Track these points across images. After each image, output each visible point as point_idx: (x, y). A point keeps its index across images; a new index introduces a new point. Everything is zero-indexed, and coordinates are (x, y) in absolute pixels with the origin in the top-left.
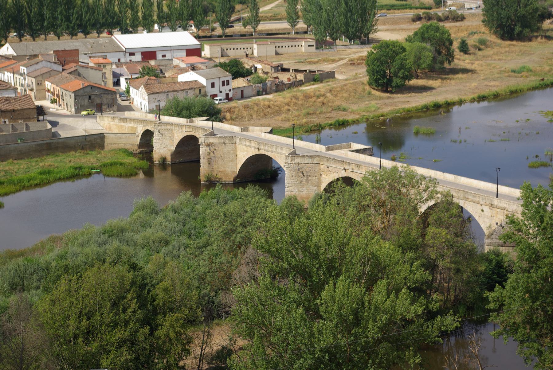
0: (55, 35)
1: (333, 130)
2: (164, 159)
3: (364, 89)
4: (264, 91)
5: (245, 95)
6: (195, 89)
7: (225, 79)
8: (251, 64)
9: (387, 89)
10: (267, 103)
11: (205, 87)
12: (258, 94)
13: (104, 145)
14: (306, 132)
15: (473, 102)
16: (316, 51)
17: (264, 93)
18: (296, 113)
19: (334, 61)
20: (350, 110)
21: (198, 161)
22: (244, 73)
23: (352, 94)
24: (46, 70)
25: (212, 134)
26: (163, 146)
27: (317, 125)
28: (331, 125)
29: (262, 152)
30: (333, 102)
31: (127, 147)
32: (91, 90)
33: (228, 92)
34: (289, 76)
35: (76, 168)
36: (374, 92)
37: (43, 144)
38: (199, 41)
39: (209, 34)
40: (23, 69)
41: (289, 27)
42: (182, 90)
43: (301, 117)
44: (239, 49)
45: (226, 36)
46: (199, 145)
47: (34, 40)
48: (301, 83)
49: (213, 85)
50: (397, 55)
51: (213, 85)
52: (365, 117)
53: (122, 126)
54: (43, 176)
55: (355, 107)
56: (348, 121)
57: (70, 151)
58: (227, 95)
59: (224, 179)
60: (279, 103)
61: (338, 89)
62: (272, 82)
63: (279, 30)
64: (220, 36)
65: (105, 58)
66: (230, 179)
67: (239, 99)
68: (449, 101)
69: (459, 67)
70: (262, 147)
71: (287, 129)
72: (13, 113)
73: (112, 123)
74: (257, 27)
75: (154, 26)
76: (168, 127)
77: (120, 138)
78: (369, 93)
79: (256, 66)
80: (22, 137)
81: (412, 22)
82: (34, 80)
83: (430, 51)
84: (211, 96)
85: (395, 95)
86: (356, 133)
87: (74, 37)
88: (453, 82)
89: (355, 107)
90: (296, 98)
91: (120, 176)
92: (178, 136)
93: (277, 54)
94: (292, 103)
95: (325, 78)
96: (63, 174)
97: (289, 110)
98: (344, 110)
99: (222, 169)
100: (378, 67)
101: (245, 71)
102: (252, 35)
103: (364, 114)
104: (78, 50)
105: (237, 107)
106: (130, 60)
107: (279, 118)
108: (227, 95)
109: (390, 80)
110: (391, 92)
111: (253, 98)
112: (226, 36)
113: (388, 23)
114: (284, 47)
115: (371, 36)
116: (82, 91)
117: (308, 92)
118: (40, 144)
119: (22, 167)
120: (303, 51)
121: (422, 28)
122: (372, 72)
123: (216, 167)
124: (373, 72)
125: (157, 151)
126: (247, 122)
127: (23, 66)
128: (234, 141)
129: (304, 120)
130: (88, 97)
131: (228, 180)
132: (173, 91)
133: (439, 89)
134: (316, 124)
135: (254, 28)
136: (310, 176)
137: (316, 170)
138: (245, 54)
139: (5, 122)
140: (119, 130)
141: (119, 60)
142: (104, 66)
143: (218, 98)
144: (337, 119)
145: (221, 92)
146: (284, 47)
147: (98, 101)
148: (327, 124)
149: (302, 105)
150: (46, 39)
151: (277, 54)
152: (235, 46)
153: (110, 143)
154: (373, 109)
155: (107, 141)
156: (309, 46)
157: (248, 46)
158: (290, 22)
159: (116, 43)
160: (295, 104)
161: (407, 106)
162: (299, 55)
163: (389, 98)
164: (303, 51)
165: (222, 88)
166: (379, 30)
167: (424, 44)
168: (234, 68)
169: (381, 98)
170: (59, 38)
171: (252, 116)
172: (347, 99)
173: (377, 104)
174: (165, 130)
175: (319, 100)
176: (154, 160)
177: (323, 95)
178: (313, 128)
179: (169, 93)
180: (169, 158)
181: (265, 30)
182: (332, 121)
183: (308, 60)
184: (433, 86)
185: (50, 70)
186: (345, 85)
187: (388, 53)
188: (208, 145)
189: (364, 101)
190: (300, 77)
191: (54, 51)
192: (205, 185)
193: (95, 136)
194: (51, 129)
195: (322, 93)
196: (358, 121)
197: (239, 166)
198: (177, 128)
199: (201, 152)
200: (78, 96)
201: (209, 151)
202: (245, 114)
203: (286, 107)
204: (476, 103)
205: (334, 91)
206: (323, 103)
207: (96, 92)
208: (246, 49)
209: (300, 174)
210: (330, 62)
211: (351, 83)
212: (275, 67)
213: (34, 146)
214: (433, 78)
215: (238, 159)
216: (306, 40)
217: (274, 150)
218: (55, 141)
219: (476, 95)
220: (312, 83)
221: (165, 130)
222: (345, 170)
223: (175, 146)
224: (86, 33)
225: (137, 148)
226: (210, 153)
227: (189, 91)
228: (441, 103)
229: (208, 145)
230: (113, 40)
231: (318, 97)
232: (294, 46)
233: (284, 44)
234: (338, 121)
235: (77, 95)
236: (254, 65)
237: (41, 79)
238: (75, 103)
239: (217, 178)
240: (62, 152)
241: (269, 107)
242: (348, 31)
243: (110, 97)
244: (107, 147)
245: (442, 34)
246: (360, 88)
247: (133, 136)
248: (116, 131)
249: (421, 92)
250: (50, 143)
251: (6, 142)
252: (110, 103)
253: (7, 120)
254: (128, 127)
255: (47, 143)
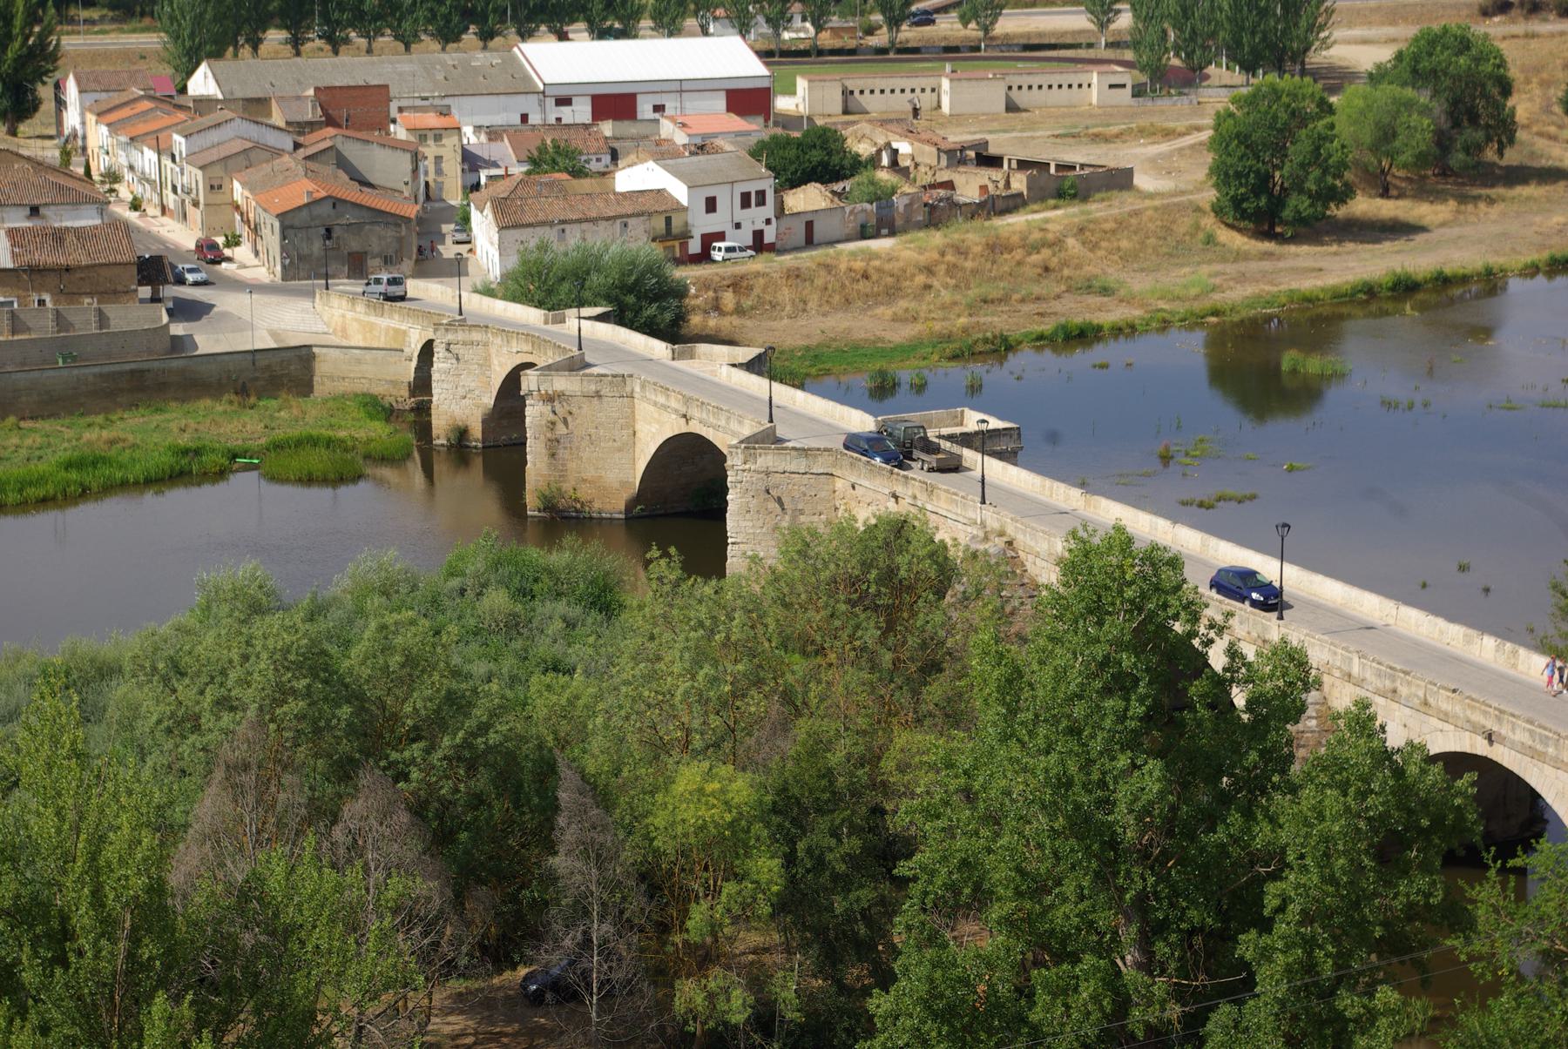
0: (396, 38)
1: (1048, 353)
2: (462, 433)
3: (1197, 227)
4: (884, 225)
5: (817, 237)
6: (650, 214)
7: (753, 187)
8: (881, 141)
9: (1272, 227)
10: (859, 265)
11: (685, 209)
12: (864, 234)
13: (311, 380)
14: (954, 357)
15: (1533, 275)
16: (1133, 102)
17: (884, 231)
18: (946, 296)
19: (1169, 134)
20: (1122, 292)
21: (522, 444)
22: (842, 167)
23: (1152, 241)
24: (237, 146)
25: (576, 365)
26: (461, 391)
27: (995, 337)
28: (1041, 337)
29: (695, 427)
30: (1079, 267)
31: (378, 389)
32: (332, 212)
33: (760, 226)
34: (986, 181)
35: (185, 452)
36: (1226, 236)
37: (121, 373)
38: (767, 64)
39: (852, 44)
40: (179, 142)
41: (1092, 26)
42: (608, 219)
43: (956, 310)
44: (1055, 87)
45: (900, 51)
46: (523, 399)
47: (336, 53)
48: (1013, 204)
49: (711, 205)
50: (1303, 124)
51: (711, 205)
52: (1160, 315)
53: (372, 326)
54: (74, 475)
55: (1139, 283)
56: (1099, 328)
57: (199, 398)
58: (758, 235)
59: (597, 505)
60: (901, 264)
61: (1108, 226)
62: (914, 198)
63: (1064, 34)
64: (882, 51)
65: (445, 112)
66: (616, 505)
67: (797, 249)
68: (1448, 271)
69: (1543, 163)
70: (694, 412)
71: (893, 349)
72: (66, 276)
73: (349, 315)
74: (992, 23)
75: (278, 27)
76: (476, 336)
77: (359, 361)
78: (1210, 240)
79: (895, 145)
80: (67, 349)
81: (1480, 18)
82: (200, 173)
83: (1425, 111)
84: (704, 236)
85: (1293, 248)
86: (1103, 366)
87: (451, 46)
88: (1495, 211)
89: (1139, 283)
90: (962, 251)
91: (309, 480)
92: (501, 365)
93: (1011, 107)
94: (943, 267)
95: (1099, 190)
96: (135, 473)
97: (928, 287)
98: (1105, 291)
99: (590, 473)
100: (1241, 158)
101: (846, 163)
102: (978, 49)
103: (1162, 305)
104: (386, 87)
105: (764, 275)
106: (559, 119)
107: (885, 311)
108: (758, 235)
109: (1278, 203)
110: (1281, 239)
111: (840, 246)
112: (900, 51)
113: (1405, 20)
114: (1035, 87)
115: (1316, 58)
116: (305, 213)
117: (1004, 233)
118: (114, 373)
119: (29, 442)
120: (1094, 101)
121: (1416, 40)
122: (1223, 175)
123: (572, 465)
124: (1226, 174)
125: (444, 408)
126: (786, 321)
127: (178, 133)
128: (628, 389)
129: (963, 321)
130: (322, 231)
131: (608, 507)
132: (579, 221)
133: (1442, 230)
134: (989, 335)
135: (986, 30)
136: (802, 512)
137: (822, 494)
138: (909, 108)
139: (42, 302)
140: (365, 339)
141: (524, 118)
142: (438, 138)
143: (722, 245)
144: (1063, 320)
145: (738, 226)
146: (1035, 87)
147: (355, 245)
148: (1026, 335)
149: (974, 272)
150: (369, 51)
151: (1011, 107)
152: (887, 83)
153: (329, 374)
154: (1193, 292)
155: (322, 368)
156: (1111, 86)
157: (928, 82)
158: (1092, 13)
159: (521, 67)
160: (952, 269)
161: (1308, 284)
162: (1078, 114)
163: (1267, 255)
164: (1094, 101)
165: (742, 215)
166: (1335, 42)
167: (1409, 92)
168: (814, 152)
169: (1240, 256)
170: (407, 48)
171: (805, 303)
172: (1126, 258)
173: (1217, 274)
174: (464, 344)
175: (1035, 258)
176: (435, 432)
177: (1051, 245)
178: (980, 347)
179: (567, 227)
180: (476, 431)
181: (1022, 36)
182: (1047, 327)
183: (1091, 131)
184: (1425, 222)
185: (249, 145)
186: (1136, 213)
187: (1275, 117)
188: (549, 399)
189: (1182, 265)
190: (1019, 183)
191: (317, 89)
192: (541, 521)
193: (284, 354)
194: (167, 326)
195: (1050, 236)
196: (1133, 327)
197: (641, 466)
198: (498, 341)
199: (528, 420)
200: (292, 227)
201: (552, 417)
202: (785, 295)
203: (921, 279)
204: (1541, 279)
205: (1093, 232)
206: (1047, 269)
207: (349, 218)
208: (918, 91)
209: (773, 506)
210: (1158, 138)
211: (1156, 209)
212: (950, 153)
213: (91, 379)
214: (1435, 196)
215: (638, 446)
216: (1105, 68)
217: (723, 423)
218: (175, 364)
219: (1542, 256)
220: (1052, 202)
221: (464, 344)
222: (896, 497)
223: (494, 394)
224: (487, 36)
225: (406, 394)
226: (553, 423)
227: (632, 222)
228: (1420, 277)
229: (549, 399)
230: (514, 59)
231: (1036, 248)
232: (1065, 87)
233: (1035, 80)
234: (1064, 327)
235: (290, 224)
236: (888, 144)
237: (222, 174)
238: (283, 249)
239: (577, 500)
240: (176, 399)
241: (866, 276)
242: (1239, 44)
243: (390, 233)
244: (322, 387)
245: (1477, 60)
246: (1184, 225)
247: (395, 356)
248: (357, 340)
249: (1377, 241)
250: (142, 371)
251: (23, 364)
252: (391, 252)
253: (47, 297)
254: (388, 329)
255: (132, 372)
